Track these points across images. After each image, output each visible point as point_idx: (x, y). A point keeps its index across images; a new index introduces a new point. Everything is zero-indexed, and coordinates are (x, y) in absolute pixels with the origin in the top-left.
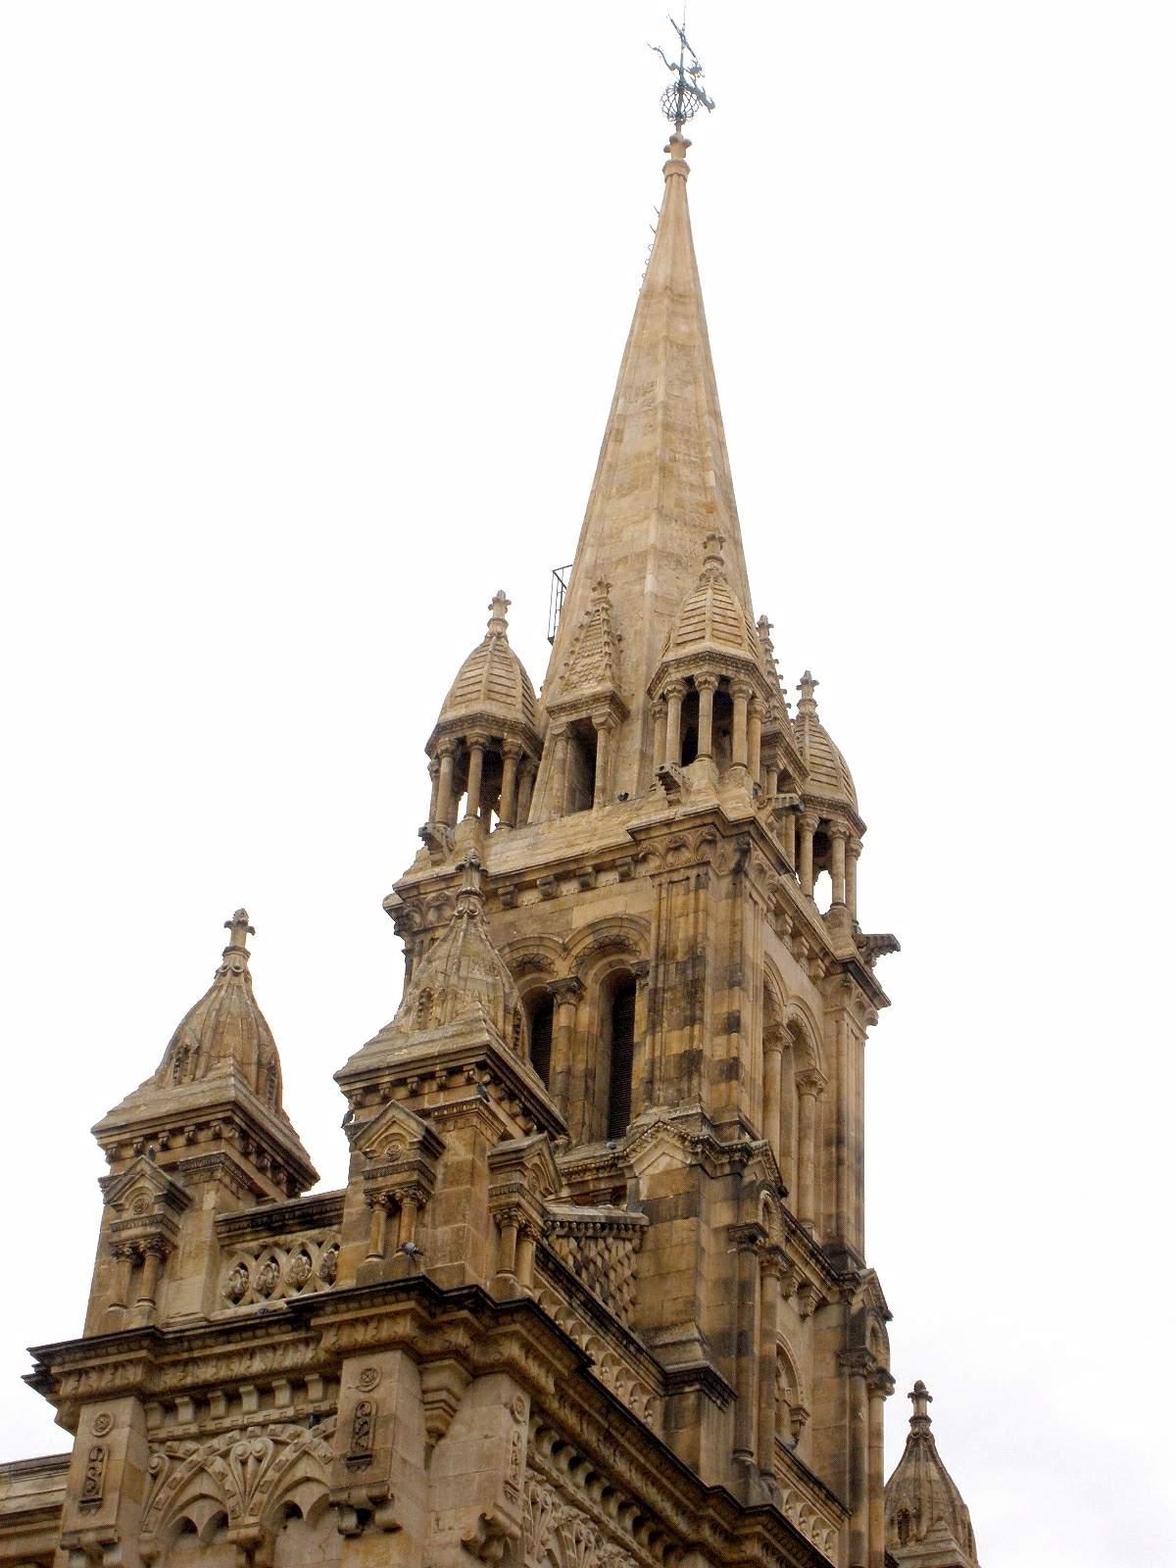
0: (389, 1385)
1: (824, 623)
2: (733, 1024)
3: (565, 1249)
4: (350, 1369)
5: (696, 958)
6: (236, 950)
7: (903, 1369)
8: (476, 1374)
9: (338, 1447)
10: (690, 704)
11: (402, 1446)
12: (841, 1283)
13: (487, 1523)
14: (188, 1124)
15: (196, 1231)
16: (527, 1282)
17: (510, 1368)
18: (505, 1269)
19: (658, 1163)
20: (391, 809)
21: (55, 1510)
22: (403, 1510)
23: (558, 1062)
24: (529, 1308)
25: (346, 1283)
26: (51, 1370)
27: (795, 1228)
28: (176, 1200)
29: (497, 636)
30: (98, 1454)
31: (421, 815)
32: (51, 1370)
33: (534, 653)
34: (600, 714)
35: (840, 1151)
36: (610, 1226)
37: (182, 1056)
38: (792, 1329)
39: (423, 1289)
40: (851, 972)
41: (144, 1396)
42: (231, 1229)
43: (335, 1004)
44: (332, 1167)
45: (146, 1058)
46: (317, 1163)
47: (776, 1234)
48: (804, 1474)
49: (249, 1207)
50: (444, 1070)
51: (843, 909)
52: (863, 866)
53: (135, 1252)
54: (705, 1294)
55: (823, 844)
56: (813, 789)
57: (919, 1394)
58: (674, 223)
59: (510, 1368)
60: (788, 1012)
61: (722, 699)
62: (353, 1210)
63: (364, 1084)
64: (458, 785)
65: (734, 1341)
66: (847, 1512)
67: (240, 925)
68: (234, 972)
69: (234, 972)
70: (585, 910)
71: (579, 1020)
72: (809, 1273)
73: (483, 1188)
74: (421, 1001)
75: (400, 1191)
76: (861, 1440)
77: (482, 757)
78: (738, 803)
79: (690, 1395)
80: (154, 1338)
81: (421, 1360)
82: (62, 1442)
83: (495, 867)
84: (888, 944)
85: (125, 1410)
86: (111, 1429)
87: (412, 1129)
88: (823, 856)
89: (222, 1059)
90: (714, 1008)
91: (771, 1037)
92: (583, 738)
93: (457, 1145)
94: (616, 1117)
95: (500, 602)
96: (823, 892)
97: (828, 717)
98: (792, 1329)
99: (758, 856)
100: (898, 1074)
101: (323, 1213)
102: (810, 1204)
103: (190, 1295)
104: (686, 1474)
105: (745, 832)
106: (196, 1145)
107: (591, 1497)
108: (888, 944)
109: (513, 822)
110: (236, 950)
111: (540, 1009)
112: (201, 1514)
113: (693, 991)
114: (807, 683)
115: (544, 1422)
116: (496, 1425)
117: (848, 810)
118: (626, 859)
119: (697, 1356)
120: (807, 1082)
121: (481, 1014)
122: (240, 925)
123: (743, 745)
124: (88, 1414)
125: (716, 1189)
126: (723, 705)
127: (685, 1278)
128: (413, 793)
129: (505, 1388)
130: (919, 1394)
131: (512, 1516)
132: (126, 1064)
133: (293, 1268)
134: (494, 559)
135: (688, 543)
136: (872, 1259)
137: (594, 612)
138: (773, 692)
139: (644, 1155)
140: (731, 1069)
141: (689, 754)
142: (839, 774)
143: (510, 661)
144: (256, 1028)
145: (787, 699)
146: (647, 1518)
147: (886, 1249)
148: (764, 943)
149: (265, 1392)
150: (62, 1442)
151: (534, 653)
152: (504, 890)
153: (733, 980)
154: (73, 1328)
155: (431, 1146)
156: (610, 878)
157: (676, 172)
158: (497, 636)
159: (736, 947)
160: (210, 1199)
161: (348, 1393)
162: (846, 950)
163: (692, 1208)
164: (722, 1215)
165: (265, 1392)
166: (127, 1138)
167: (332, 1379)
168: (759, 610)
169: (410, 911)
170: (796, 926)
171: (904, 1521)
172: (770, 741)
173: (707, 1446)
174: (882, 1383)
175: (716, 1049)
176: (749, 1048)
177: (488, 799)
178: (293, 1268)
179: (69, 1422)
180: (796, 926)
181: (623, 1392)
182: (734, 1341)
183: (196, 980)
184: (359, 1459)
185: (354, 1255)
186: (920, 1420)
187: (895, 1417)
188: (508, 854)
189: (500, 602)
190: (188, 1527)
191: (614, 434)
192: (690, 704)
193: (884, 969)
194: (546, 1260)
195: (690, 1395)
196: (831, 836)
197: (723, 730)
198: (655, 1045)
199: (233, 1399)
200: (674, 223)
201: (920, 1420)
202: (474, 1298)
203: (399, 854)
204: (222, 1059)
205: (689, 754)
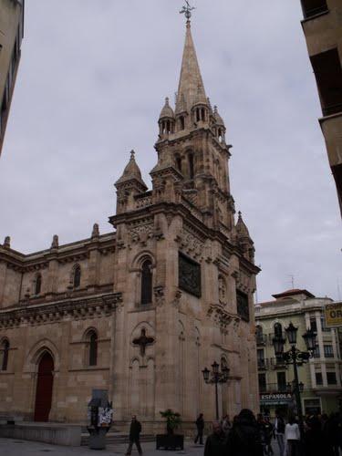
0: (163, 218)
1: (215, 96)
2: (208, 160)
3: (186, 196)
4: (156, 217)
5: (202, 151)
6: (132, 156)
7: (237, 209)
8: (174, 215)
9: (155, 228)
10: (198, 112)
11: (164, 226)
12: (227, 198)
13: (178, 237)
14: (128, 182)
15: (130, 198)
16: (180, 201)
17: (179, 214)
18: (177, 199)
19: (198, 182)
20: (153, 133)
21: (115, 240)
22: (165, 236)
23: (182, 168)
24: (181, 205)
25: (154, 203)
26: (112, 220)
27: (219, 190)
28: (127, 194)
29: (167, 104)
30: (120, 231)
31: (158, 132)
32: (112, 220)
33: (173, 106)
34: (184, 115)
35: (226, 179)
36: (192, 192)
37: (126, 172)
38: (223, 207)
39: (165, 204)
40: (225, 151)
41: (126, 223)
42: (136, 198)
43: (148, 163)
44: (150, 187)
45: (121, 174)
46: (148, 186)
47: (217, 191)
48: (223, 225)
49: (138, 194)
50: (165, 171)
51: (223, 142)
52: (226, 135)
53: (122, 202)
54: (207, 201)
55: (220, 131)
56: (217, 123)
57: (240, 213)
58: (188, 35)
59: (179, 214)
60: (216, 158)
61: (202, 110)
62: (153, 193)
63: (153, 174)
64: (163, 128)
65: (212, 207)
66: (230, 231)
67: (133, 152)
68: (132, 159)
69: (132, 159)
70: (187, 144)
71: (185, 161)
72: (222, 196)
73: (173, 188)
74: (161, 161)
75: (159, 189)
76: (231, 220)
77: (166, 123)
78: (206, 126)
79: (206, 216)
80: (126, 214)
81: (166, 214)
82: (115, 230)
83: (170, 140)
84: (231, 146)
85: (123, 225)
86: (137, 256)
87: (161, 181)
88: (220, 135)
89: (132, 171)
90: (205, 158)
91: (214, 162)
92: (182, 119)
93: (168, 182)
94: (192, 175)
95: (167, 99)
96: (220, 139)
97: (219, 112)
98: (223, 207)
99: (210, 135)
100: (234, 166)
101: (150, 193)
102: (221, 186)
103: (132, 206)
104: (206, 228)
105: (208, 131)
106: (129, 185)
107: (192, 231)
108: (231, 146)
109: (172, 133)
110: (132, 156)
111: (179, 161)
112: (136, 239)
113: (202, 156)
114: (215, 107)
115: (185, 222)
116: (177, 223)
117: (223, 126)
118: (190, 137)
119: (206, 210)
120: (220, 168)
121: (170, 161)
122: (133, 152)
123: (207, 118)
124: (118, 226)
125: (207, 185)
126: (203, 111)
127: (203, 199)
128: (156, 129)
129: (179, 217)
130: (240, 213)
131: (181, 235)
132: (118, 174)
133: (146, 202)
134: (164, 91)
135: (196, 87)
136: (232, 193)
137: (181, 98)
138: (210, 109)
139: (115, 344)
140: (208, 167)
141: (198, 119)
142: (221, 121)
143: (169, 107)
144: (137, 167)
145: (120, 353)
146: (201, 234)
147: (232, 193)
148: (211, 147)
149: (144, 221)
150: (115, 230)
151: (173, 106)
152: (172, 143)
153: (208, 153)
154: (114, 214)
155: (164, 183)
156: (187, 140)
157: (188, 27)
158: (167, 104)
159: (207, 149)
160: (133, 193)
161: (155, 220)
162: (224, 148)
163: (204, 188)
164: (208, 189)
165: (144, 221)
166: (119, 185)
167: (153, 218)
168: (207, 95)
169: (158, 148)
170: (216, 144)
171: (238, 231)
172: (211, 116)
173: (209, 223)
174: (234, 212)
175: (205, 164)
176: (211, 164)
177: (168, 129)
178: (146, 202)
179: (115, 227)
180: (216, 144)
181: (196, 216)
182: (212, 207)
183: (126, 162)
184: (158, 229)
185: (154, 200)
186: (240, 217)
187: (236, 217)
188: (171, 138)
189: (167, 99)
190: (134, 241)
191: (182, 70)
192: (198, 112)
193: (230, 150)
194: (183, 198)
195: (206, 216)
196: (221, 130)
197: (203, 115)
198: (197, 164)
199: (139, 222)
200: (188, 35)
201: (240, 217)
202: (173, 204)
203: (156, 139)
204: (132, 171)
205: (198, 119)
